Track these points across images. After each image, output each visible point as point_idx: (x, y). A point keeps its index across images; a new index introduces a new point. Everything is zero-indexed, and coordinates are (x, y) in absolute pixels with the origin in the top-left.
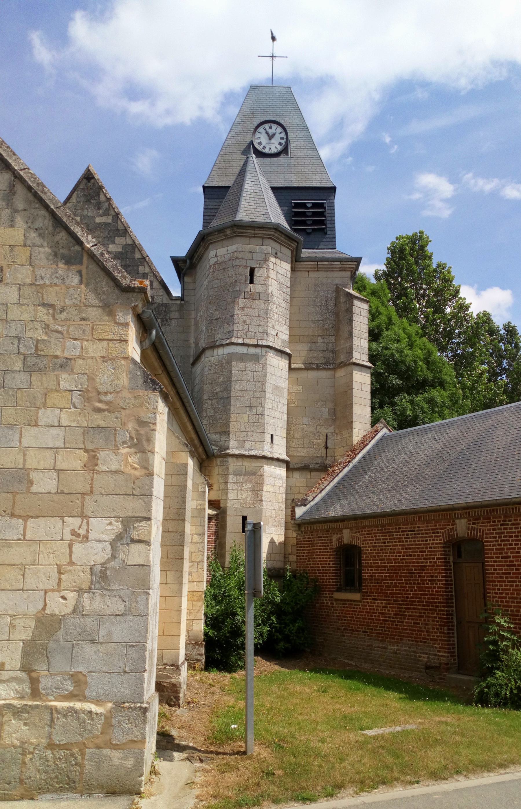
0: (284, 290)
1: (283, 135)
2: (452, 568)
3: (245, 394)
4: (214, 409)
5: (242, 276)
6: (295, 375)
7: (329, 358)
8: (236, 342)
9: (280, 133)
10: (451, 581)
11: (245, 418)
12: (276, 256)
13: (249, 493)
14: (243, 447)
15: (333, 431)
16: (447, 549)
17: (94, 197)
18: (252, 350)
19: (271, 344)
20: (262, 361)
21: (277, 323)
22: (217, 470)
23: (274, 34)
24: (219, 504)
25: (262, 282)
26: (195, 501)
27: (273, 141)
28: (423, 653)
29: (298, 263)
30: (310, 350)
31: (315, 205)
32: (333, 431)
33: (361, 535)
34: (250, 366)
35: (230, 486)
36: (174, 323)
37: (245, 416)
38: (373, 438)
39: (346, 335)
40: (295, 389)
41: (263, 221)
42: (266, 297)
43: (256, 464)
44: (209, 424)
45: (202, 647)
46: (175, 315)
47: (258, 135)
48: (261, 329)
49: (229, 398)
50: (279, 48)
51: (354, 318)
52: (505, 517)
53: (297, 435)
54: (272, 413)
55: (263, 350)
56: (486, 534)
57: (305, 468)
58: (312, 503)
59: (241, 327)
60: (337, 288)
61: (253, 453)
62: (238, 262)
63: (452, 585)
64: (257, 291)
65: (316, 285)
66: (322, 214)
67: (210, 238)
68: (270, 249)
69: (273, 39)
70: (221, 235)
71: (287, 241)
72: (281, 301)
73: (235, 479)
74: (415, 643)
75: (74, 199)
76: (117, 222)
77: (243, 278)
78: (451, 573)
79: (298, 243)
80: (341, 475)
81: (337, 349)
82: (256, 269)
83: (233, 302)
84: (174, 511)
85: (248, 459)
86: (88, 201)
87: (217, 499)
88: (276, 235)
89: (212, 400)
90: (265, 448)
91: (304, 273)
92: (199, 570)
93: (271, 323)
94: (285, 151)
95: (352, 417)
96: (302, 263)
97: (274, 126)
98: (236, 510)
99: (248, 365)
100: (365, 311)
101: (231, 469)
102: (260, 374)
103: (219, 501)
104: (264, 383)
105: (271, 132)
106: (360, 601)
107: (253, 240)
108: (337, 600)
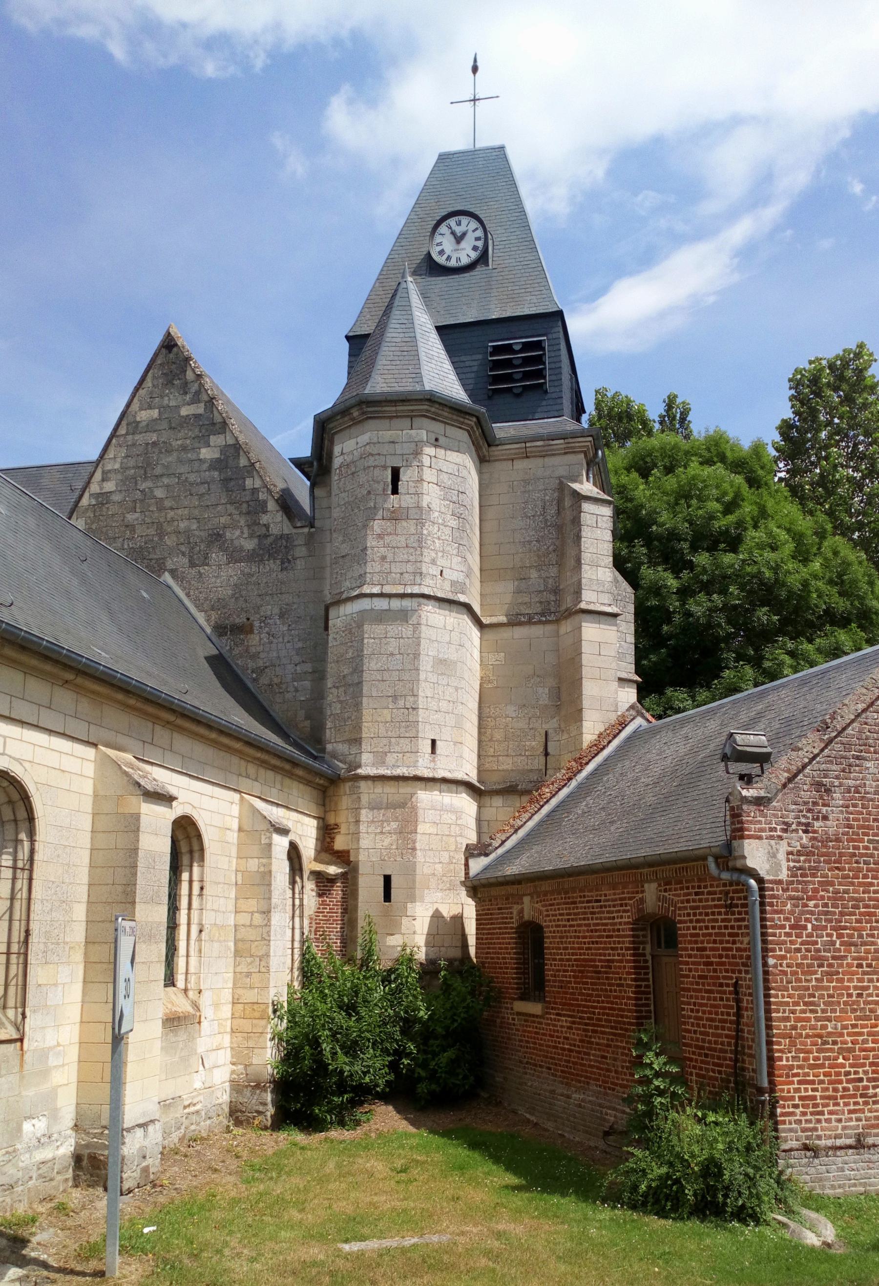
0: (455, 498)
1: (480, 233)
2: (650, 964)
3: (386, 675)
4: (341, 702)
5: (378, 482)
6: (491, 635)
7: (549, 603)
8: (368, 591)
9: (474, 231)
10: (647, 986)
11: (387, 714)
12: (436, 443)
13: (394, 837)
14: (383, 763)
15: (556, 726)
16: (641, 933)
17: (178, 375)
18: (396, 604)
19: (426, 591)
20: (413, 620)
21: (440, 554)
22: (345, 802)
23: (479, 64)
24: (349, 856)
25: (412, 491)
26: (256, 860)
27: (463, 244)
28: (609, 1108)
29: (494, 448)
30: (518, 592)
31: (527, 347)
32: (556, 726)
33: (543, 906)
34: (393, 629)
35: (363, 828)
36: (300, 564)
37: (386, 711)
38: (615, 737)
39: (573, 562)
40: (492, 659)
41: (410, 389)
42: (420, 515)
43: (405, 789)
44: (336, 727)
45: (266, 1091)
46: (301, 551)
47: (438, 239)
48: (410, 568)
49: (360, 683)
50: (485, 84)
51: (583, 534)
52: (700, 880)
53: (498, 735)
54: (433, 705)
55: (415, 601)
56: (680, 909)
57: (510, 790)
58: (500, 851)
59: (377, 567)
60: (561, 483)
61: (398, 772)
62: (371, 461)
63: (649, 993)
64: (404, 505)
65: (526, 482)
66: (539, 360)
67: (331, 425)
68: (423, 435)
69: (475, 69)
70: (346, 419)
71: (455, 417)
72: (449, 517)
73: (370, 816)
74: (602, 1090)
75: (148, 383)
76: (212, 412)
77: (380, 487)
78: (647, 974)
79: (478, 418)
80: (554, 802)
81: (561, 587)
82: (402, 470)
83: (365, 526)
84: (120, 889)
85: (392, 783)
86: (169, 383)
87: (345, 848)
88: (433, 409)
89: (337, 688)
90: (421, 762)
91: (505, 463)
92: (263, 970)
93: (428, 555)
94: (483, 258)
95: (581, 701)
96: (500, 448)
97: (465, 220)
98: (373, 866)
99: (389, 628)
100: (605, 519)
101: (365, 799)
102: (411, 641)
103: (348, 852)
104: (416, 656)
105: (459, 230)
106: (541, 1017)
107: (396, 422)
108: (519, 1014)
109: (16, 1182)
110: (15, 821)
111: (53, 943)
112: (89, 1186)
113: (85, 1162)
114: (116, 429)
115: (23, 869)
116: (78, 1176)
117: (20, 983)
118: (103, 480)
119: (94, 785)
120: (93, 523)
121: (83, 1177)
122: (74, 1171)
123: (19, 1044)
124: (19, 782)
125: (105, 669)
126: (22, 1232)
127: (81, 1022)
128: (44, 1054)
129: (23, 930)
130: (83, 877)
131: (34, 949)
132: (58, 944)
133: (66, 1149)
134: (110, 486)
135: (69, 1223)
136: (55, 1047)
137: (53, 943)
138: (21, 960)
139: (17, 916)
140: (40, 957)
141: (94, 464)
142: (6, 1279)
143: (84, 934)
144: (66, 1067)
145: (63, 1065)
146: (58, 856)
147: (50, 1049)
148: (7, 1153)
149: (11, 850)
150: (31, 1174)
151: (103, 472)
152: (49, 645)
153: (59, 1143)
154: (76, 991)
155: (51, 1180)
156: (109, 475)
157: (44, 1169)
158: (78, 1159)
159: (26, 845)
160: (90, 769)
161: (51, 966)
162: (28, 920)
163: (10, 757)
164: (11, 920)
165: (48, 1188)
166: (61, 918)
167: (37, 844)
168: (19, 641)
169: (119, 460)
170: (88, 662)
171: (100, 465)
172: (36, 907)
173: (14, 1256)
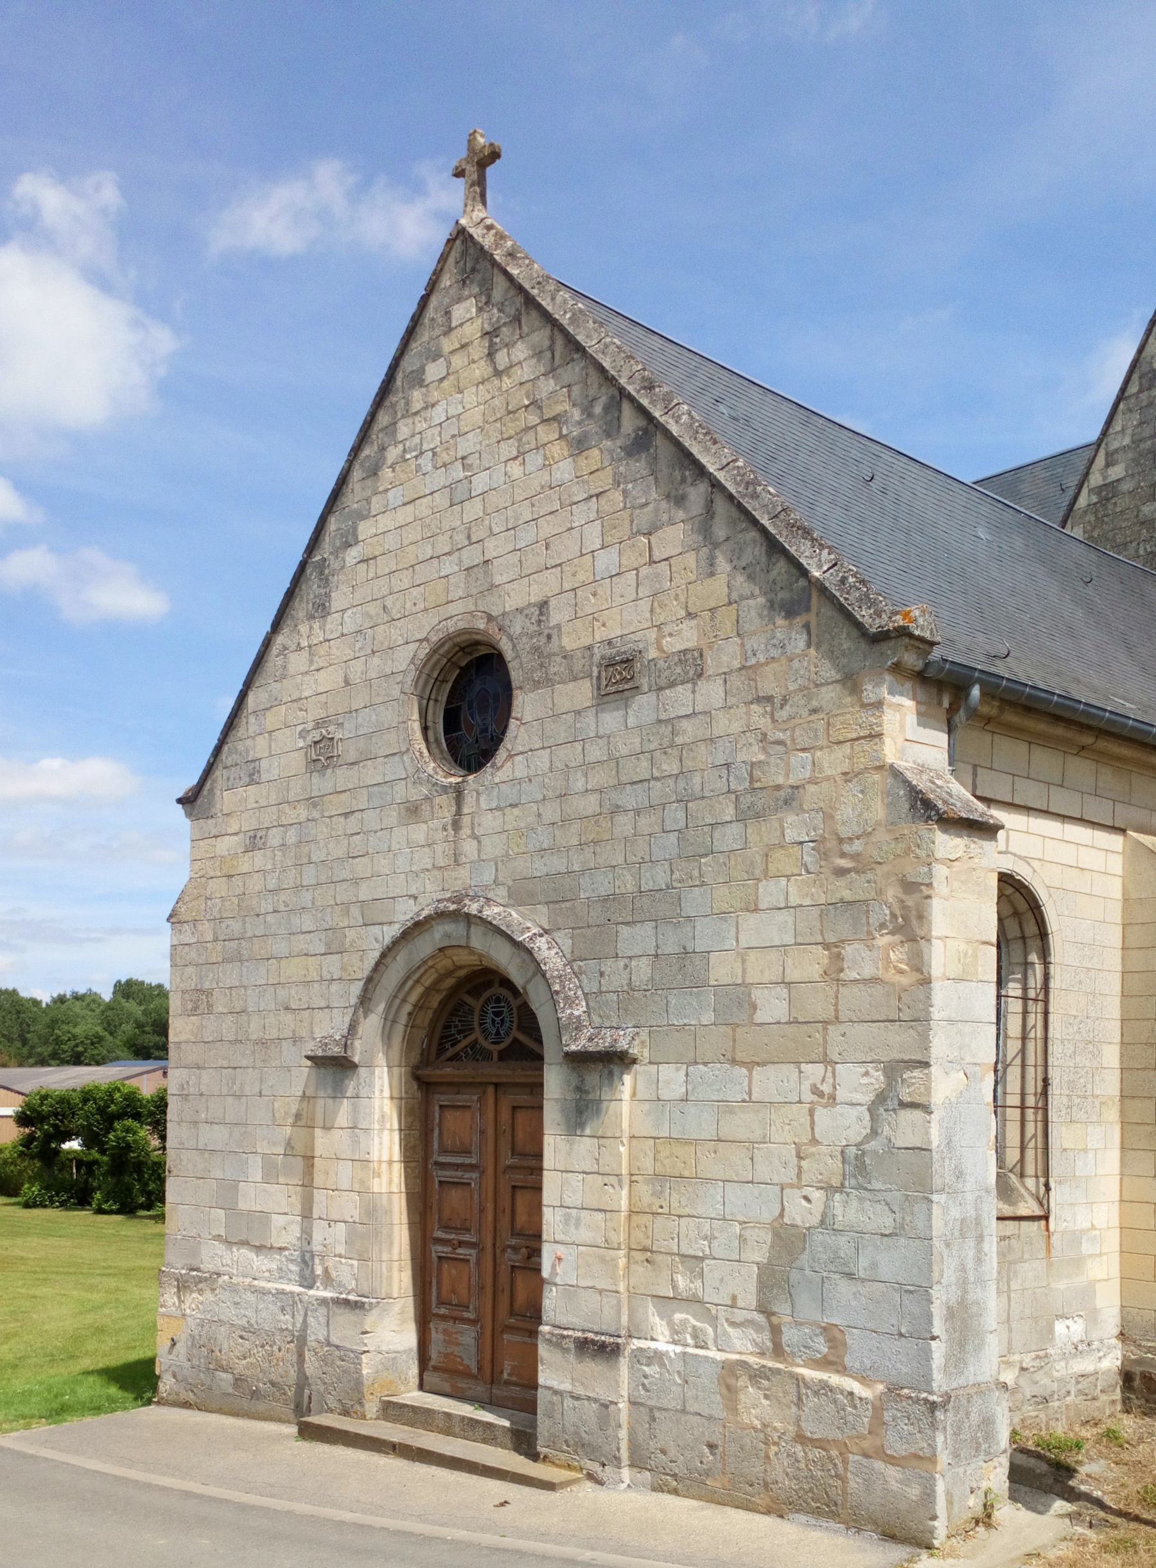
109: (1052, 1395)
110: (1023, 938)
111: (1078, 1096)
112: (1145, 1414)
113: (1137, 1383)
114: (1123, 389)
115: (1036, 1000)
116: (1129, 1398)
117: (1040, 1145)
118: (1108, 465)
119: (1124, 885)
120: (1094, 528)
121: (1135, 1401)
122: (1122, 1392)
123: (1043, 1222)
124: (1026, 887)
125: (1136, 724)
126: (1069, 1459)
127: (1121, 1201)
128: (1076, 1238)
129: (1040, 1077)
130: (1113, 1008)
131: (1055, 1103)
132: (1085, 1097)
133: (1111, 1361)
134: (1117, 472)
135: (1125, 1456)
136: (1088, 1230)
137: (1078, 1096)
138: (1040, 1117)
139: (1031, 1060)
140: (1063, 1113)
141: (1094, 447)
142: (1052, 1512)
143: (1118, 1085)
144: (1105, 1258)
145: (1101, 1254)
146: (1080, 983)
147: (1083, 1232)
148: (1038, 1357)
149: (1019, 976)
150: (1068, 1388)
151: (1107, 454)
152: (1061, 700)
153: (1101, 1354)
154: (1112, 1159)
155: (1094, 1399)
156: (1115, 456)
157: (1084, 1384)
158: (1127, 1377)
159: (1039, 969)
160: (1116, 864)
161: (1078, 1125)
162: (1046, 1066)
163: (1015, 855)
164: (1023, 1066)
165: (1090, 1410)
166: (1088, 1064)
167: (1052, 967)
168: (1023, 701)
169: (1129, 432)
170: (1114, 717)
171: (1103, 445)
172: (1055, 1049)
173: (1059, 1485)
